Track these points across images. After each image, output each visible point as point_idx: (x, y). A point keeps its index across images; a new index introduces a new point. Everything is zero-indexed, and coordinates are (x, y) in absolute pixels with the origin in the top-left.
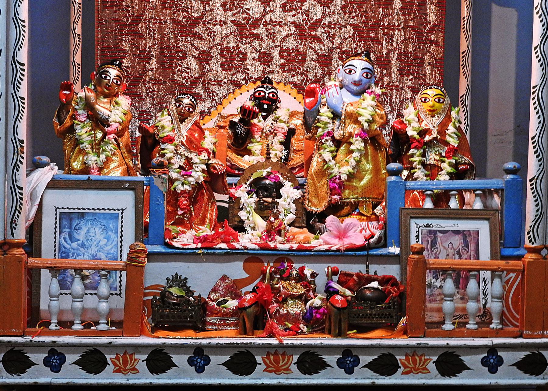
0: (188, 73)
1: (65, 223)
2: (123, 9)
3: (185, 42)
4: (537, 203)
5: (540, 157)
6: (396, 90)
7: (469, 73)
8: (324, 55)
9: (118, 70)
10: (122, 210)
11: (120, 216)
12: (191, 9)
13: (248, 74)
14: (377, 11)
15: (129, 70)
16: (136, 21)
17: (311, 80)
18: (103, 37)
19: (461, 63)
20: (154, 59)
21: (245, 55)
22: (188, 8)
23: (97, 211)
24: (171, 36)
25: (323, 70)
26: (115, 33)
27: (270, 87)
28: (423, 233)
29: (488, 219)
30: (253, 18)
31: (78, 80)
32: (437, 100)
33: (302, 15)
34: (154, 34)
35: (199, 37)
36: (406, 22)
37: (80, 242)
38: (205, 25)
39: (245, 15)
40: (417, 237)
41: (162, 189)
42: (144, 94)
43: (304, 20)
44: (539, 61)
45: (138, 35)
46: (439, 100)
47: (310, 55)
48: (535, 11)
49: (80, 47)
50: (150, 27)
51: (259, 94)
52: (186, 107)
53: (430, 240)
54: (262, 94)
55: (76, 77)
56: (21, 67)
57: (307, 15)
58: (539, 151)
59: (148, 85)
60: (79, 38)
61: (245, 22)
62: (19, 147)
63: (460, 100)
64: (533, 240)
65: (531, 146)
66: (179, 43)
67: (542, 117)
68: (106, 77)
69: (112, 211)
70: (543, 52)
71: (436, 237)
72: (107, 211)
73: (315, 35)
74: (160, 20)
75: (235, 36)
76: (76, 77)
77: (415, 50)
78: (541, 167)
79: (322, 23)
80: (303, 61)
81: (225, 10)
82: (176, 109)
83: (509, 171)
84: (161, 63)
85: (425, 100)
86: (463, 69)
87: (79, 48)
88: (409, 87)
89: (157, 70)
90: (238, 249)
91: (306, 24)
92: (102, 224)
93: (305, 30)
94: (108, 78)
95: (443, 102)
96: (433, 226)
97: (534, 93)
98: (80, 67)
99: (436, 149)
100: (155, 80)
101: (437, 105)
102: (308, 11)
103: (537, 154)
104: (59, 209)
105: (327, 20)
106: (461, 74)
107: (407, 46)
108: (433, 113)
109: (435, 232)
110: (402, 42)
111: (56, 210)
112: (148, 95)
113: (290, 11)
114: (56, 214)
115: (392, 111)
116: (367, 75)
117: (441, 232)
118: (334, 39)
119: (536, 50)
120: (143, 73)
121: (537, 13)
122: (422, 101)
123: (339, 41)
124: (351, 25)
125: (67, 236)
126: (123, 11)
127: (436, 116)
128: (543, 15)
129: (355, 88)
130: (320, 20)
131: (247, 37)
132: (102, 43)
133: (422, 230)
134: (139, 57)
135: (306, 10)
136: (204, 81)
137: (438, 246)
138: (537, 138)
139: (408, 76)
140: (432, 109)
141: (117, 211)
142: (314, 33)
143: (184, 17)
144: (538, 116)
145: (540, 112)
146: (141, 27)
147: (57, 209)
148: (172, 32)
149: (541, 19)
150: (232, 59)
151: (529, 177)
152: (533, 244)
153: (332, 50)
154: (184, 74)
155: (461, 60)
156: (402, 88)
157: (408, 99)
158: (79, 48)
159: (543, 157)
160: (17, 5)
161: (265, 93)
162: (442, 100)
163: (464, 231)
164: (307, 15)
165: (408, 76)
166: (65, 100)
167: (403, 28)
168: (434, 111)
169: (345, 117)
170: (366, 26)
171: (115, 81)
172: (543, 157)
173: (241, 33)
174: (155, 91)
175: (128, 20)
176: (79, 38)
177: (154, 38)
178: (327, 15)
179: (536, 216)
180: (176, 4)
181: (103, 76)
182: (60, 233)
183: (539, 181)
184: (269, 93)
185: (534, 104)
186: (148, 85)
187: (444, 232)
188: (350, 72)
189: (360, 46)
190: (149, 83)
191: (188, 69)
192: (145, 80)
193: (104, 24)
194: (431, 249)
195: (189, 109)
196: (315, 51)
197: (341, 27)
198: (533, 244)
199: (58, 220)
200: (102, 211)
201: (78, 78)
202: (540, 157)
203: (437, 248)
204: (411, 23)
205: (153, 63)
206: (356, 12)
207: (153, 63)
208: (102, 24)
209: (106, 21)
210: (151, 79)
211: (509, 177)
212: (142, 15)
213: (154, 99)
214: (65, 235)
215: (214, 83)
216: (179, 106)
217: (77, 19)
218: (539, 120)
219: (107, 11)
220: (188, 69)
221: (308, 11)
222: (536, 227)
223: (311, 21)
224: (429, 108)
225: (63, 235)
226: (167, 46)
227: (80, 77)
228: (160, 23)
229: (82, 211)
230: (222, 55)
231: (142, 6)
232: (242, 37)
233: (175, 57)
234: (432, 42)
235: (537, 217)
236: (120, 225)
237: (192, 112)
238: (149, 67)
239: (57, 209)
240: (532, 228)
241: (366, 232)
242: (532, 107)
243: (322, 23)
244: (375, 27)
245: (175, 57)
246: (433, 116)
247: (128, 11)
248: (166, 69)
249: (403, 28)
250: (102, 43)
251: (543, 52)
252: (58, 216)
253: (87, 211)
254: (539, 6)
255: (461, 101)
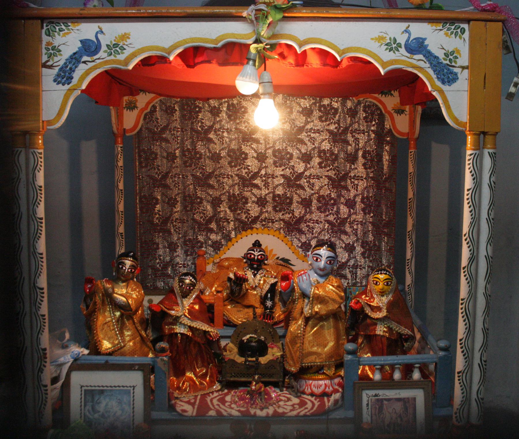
0: (204, 214)
1: (89, 398)
2: (155, 168)
3: (202, 191)
4: (463, 391)
5: (466, 356)
6: (360, 224)
7: (414, 214)
8: (306, 198)
9: (131, 261)
10: (134, 387)
11: (132, 392)
12: (206, 167)
13: (249, 214)
14: (345, 166)
15: (161, 213)
16: (165, 176)
17: (296, 217)
18: (140, 190)
19: (409, 207)
20: (179, 204)
21: (247, 199)
22: (204, 166)
23: (114, 388)
24: (191, 187)
25: (306, 210)
26: (150, 186)
27: (258, 250)
28: (373, 401)
29: (423, 388)
30: (252, 172)
31: (121, 224)
32: (386, 284)
33: (289, 169)
34: (179, 186)
35: (212, 187)
36: (367, 174)
37: (100, 413)
38: (216, 178)
39: (247, 171)
40: (368, 405)
41: (164, 369)
42: (172, 230)
43: (291, 173)
44: (467, 279)
45: (166, 187)
46: (387, 283)
47: (296, 198)
48: (464, 238)
49: (123, 199)
50: (175, 181)
51: (251, 256)
52: (187, 287)
53: (377, 407)
54: (252, 256)
55: (120, 222)
56: (41, 291)
57: (293, 170)
58: (465, 351)
59: (174, 223)
60: (122, 193)
61: (246, 175)
62: (42, 354)
63: (408, 234)
64: (459, 420)
65: (459, 346)
66: (197, 192)
67: (468, 324)
68: (122, 268)
69: (126, 388)
70: (469, 272)
71: (382, 404)
72: (122, 388)
73: (300, 184)
74: (183, 175)
75: (239, 186)
76: (120, 222)
77: (374, 195)
78: (467, 364)
79: (304, 175)
80: (291, 203)
81: (231, 167)
82: (179, 287)
83: (441, 349)
84: (185, 207)
85: (377, 283)
86: (410, 211)
87: (121, 199)
88: (370, 222)
89: (181, 212)
90: (225, 416)
91: (293, 176)
92: (118, 398)
93: (292, 181)
94: (124, 268)
95: (390, 285)
96: (380, 396)
97: (462, 304)
98: (123, 213)
99: (385, 323)
100: (180, 220)
101: (386, 287)
102: (293, 166)
103: (463, 353)
104: (84, 386)
105: (307, 173)
106: (409, 215)
107: (368, 192)
108: (383, 294)
109: (382, 400)
110: (365, 188)
111: (81, 388)
112: (175, 230)
113: (280, 167)
114: (81, 391)
115: (357, 240)
116: (330, 262)
117: (386, 400)
118: (313, 187)
119: (461, 342)
120: (171, 215)
121: (466, 240)
122: (374, 283)
123: (317, 188)
124: (326, 176)
125: (90, 409)
126: (155, 169)
127: (385, 296)
128: (470, 242)
129: (321, 273)
130: (303, 173)
131: (248, 187)
132: (140, 193)
133: (371, 399)
134: (168, 203)
135: (292, 166)
136: (217, 219)
137: (384, 411)
138: (463, 340)
139: (369, 214)
140: (382, 291)
141: (129, 388)
142: (298, 183)
143: (201, 173)
144: (464, 323)
145: (467, 320)
146: (169, 181)
147: (82, 387)
148: (192, 184)
149: (468, 245)
150: (237, 203)
151: (457, 370)
152: (459, 422)
153: (312, 194)
154: (202, 215)
155: (409, 204)
156: (365, 223)
157: (369, 231)
158: (121, 199)
159: (468, 356)
160: (35, 241)
161: (255, 255)
162: (389, 283)
163: (404, 398)
164: (293, 170)
165: (369, 214)
166: (88, 291)
167: (365, 179)
168: (383, 292)
169: (312, 299)
170: (337, 177)
171: (129, 270)
172: (468, 356)
173: (243, 184)
174: (179, 228)
175: (159, 176)
176: (122, 193)
177: (179, 189)
178: (308, 169)
179: (462, 401)
180: (195, 164)
181: (121, 266)
182: (85, 406)
183: (464, 375)
184: (258, 256)
185: (462, 313)
186: (174, 223)
187: (389, 400)
188: (317, 260)
189: (333, 192)
190: (176, 222)
191: (204, 210)
192: (173, 220)
193: (141, 179)
194: (379, 414)
195: (190, 288)
196: (299, 196)
197: (318, 177)
198: (459, 422)
199: (83, 396)
200: (117, 388)
201: (122, 222)
202: (466, 356)
203: (383, 413)
204: (371, 175)
205: (178, 208)
206: (329, 166)
207: (178, 208)
208: (139, 179)
209: (142, 177)
210: (177, 219)
211: (442, 353)
212: (169, 172)
213: (179, 234)
214: (89, 407)
215: (224, 221)
216: (182, 285)
217: (119, 178)
218: (466, 326)
219: (143, 170)
220: (204, 210)
221: (293, 166)
222: (462, 410)
223: (296, 174)
224: (379, 290)
225: (87, 408)
226: (189, 194)
227: (123, 221)
228: (183, 178)
229: (101, 388)
230: (229, 200)
231: (169, 165)
232: (244, 187)
233: (194, 203)
234: (387, 190)
235: (463, 402)
236: (132, 399)
237: (192, 290)
238: (175, 210)
239: (82, 387)
240: (458, 411)
241: (329, 388)
242: (460, 316)
243: (304, 175)
244: (345, 177)
245: (194, 203)
246: (383, 296)
247: (159, 170)
248: (188, 211)
249: (365, 179)
250: (140, 193)
251: (469, 272)
252: (83, 392)
253: (105, 388)
254: (467, 235)
255: (408, 235)
